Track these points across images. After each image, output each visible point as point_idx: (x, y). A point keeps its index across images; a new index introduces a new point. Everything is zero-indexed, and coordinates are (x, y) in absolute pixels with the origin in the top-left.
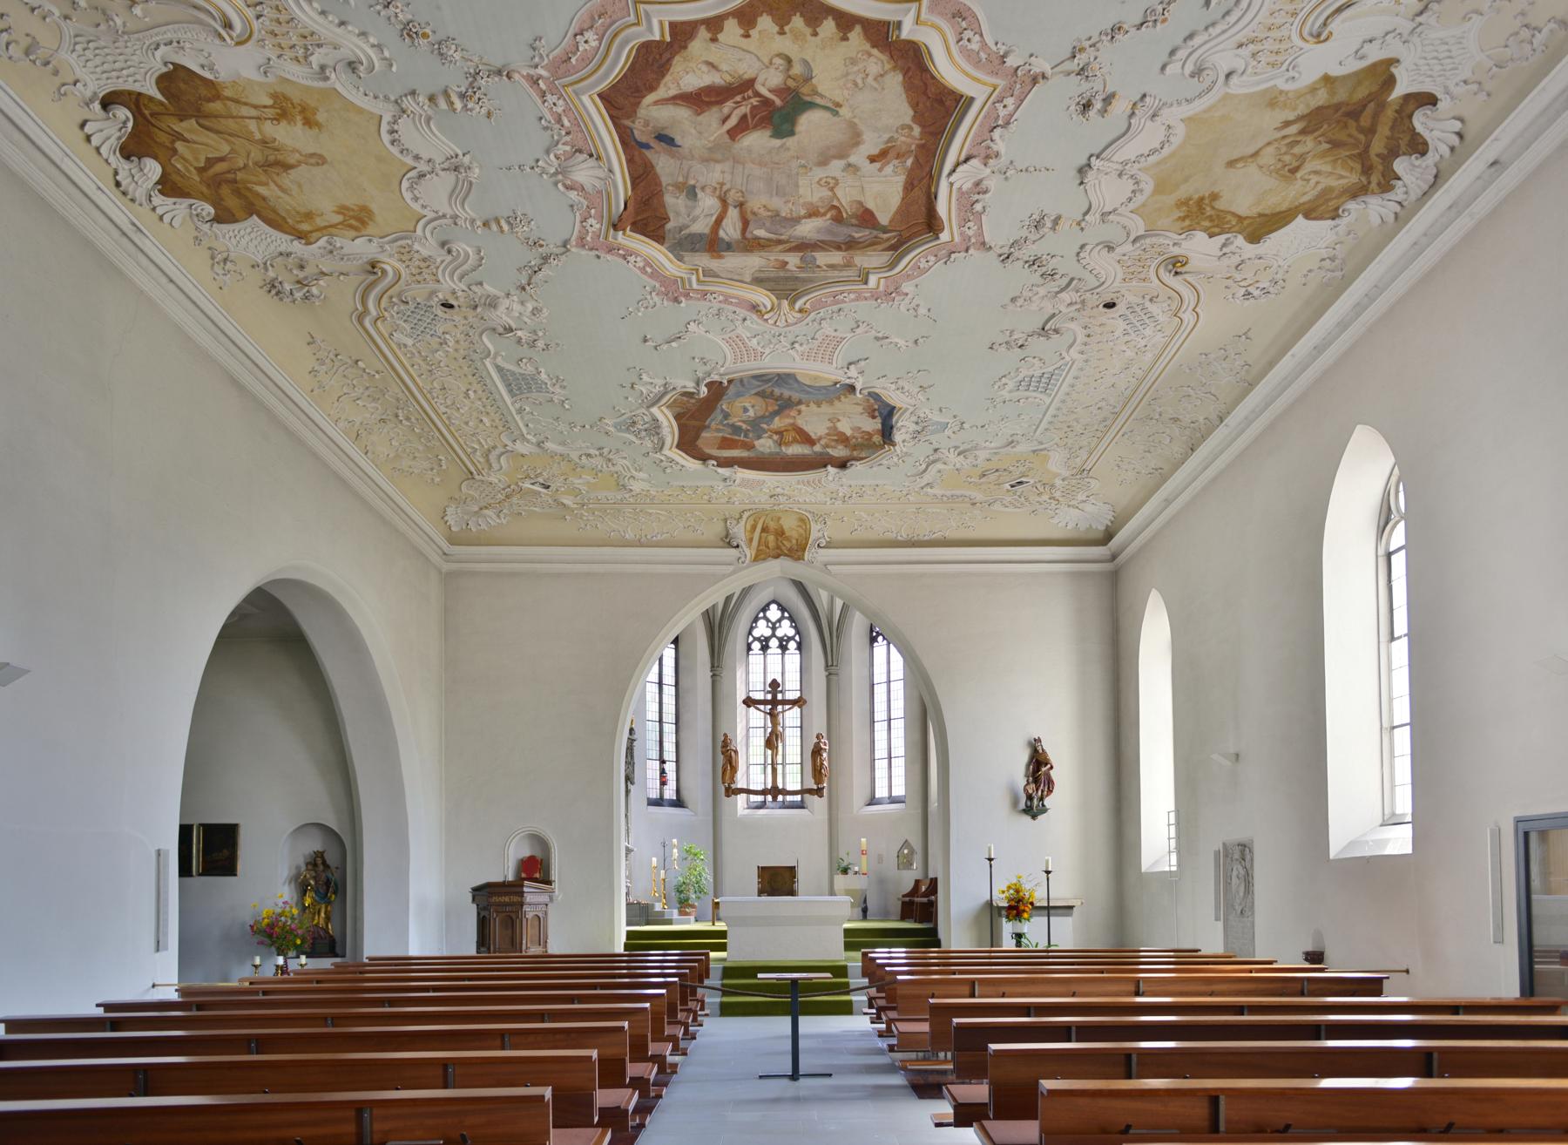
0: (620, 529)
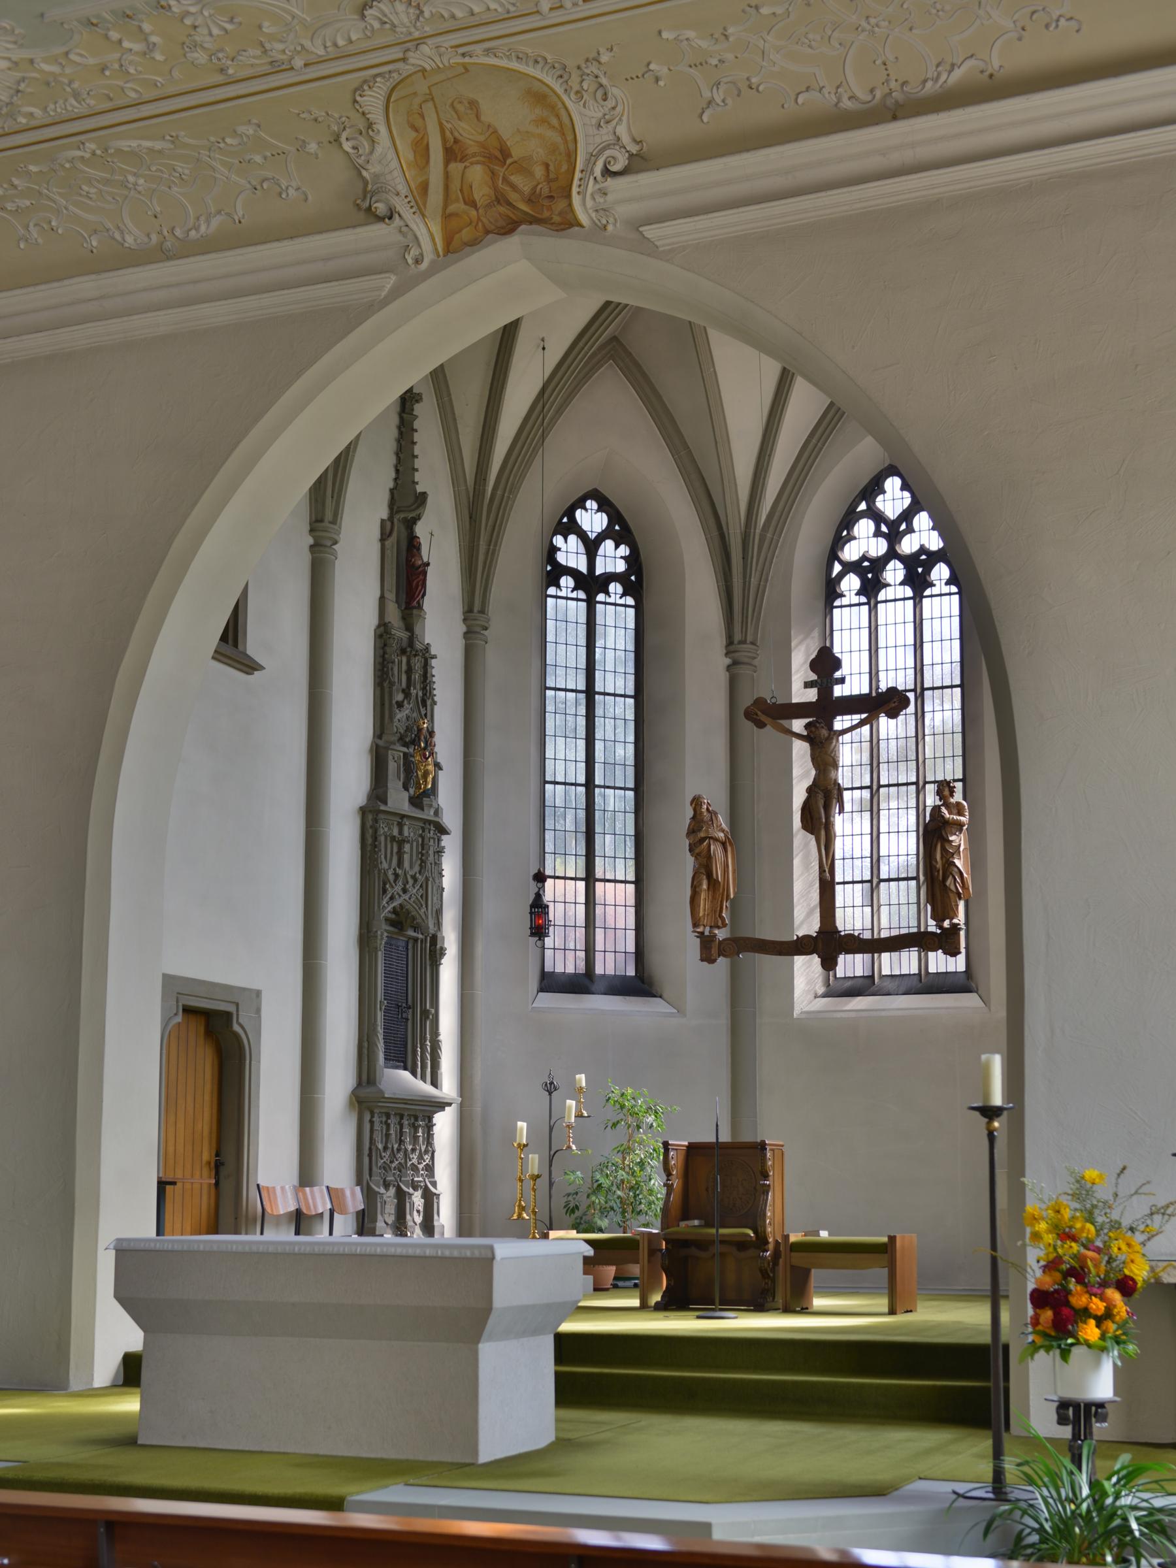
0: (110, 225)
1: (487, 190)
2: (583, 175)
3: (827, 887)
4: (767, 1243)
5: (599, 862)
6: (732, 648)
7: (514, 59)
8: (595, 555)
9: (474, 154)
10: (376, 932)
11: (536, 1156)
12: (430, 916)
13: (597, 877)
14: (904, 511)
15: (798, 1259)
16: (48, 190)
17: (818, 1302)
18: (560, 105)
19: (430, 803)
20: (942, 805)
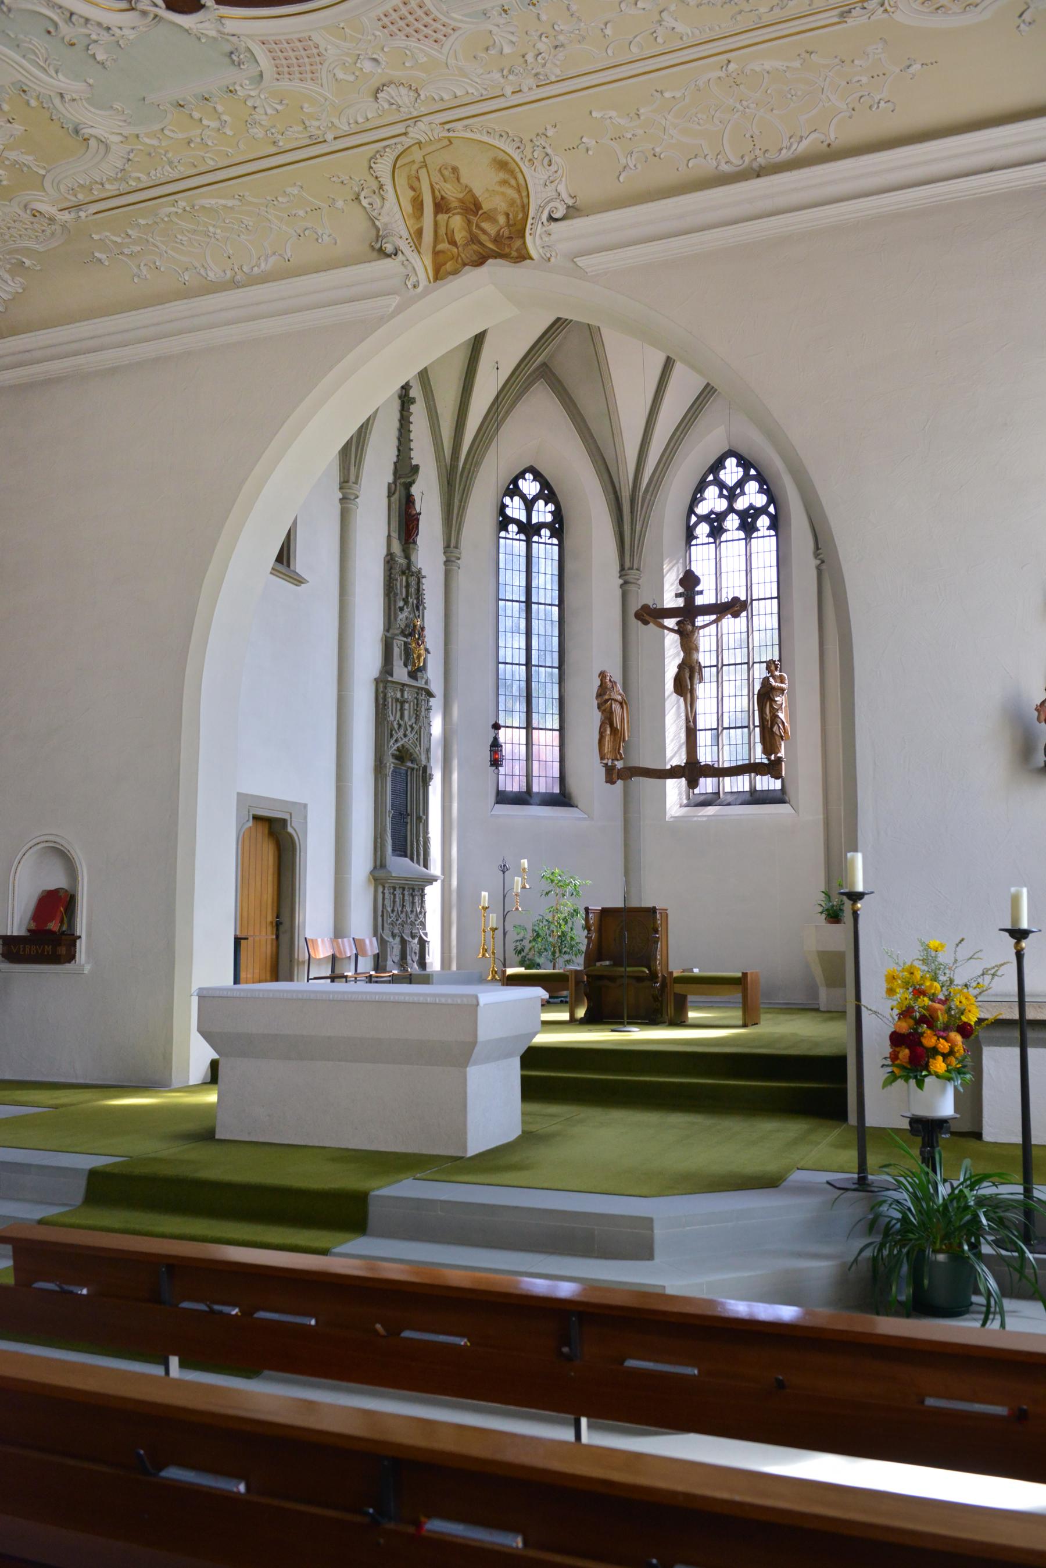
0: (197, 264)
1: (464, 233)
2: (534, 221)
3: (691, 733)
4: (658, 977)
6: (623, 573)
7: (485, 133)
8: (532, 510)
9: (455, 208)
11: (495, 915)
12: (422, 753)
15: (679, 988)
16: (153, 238)
17: (692, 1015)
18: (517, 170)
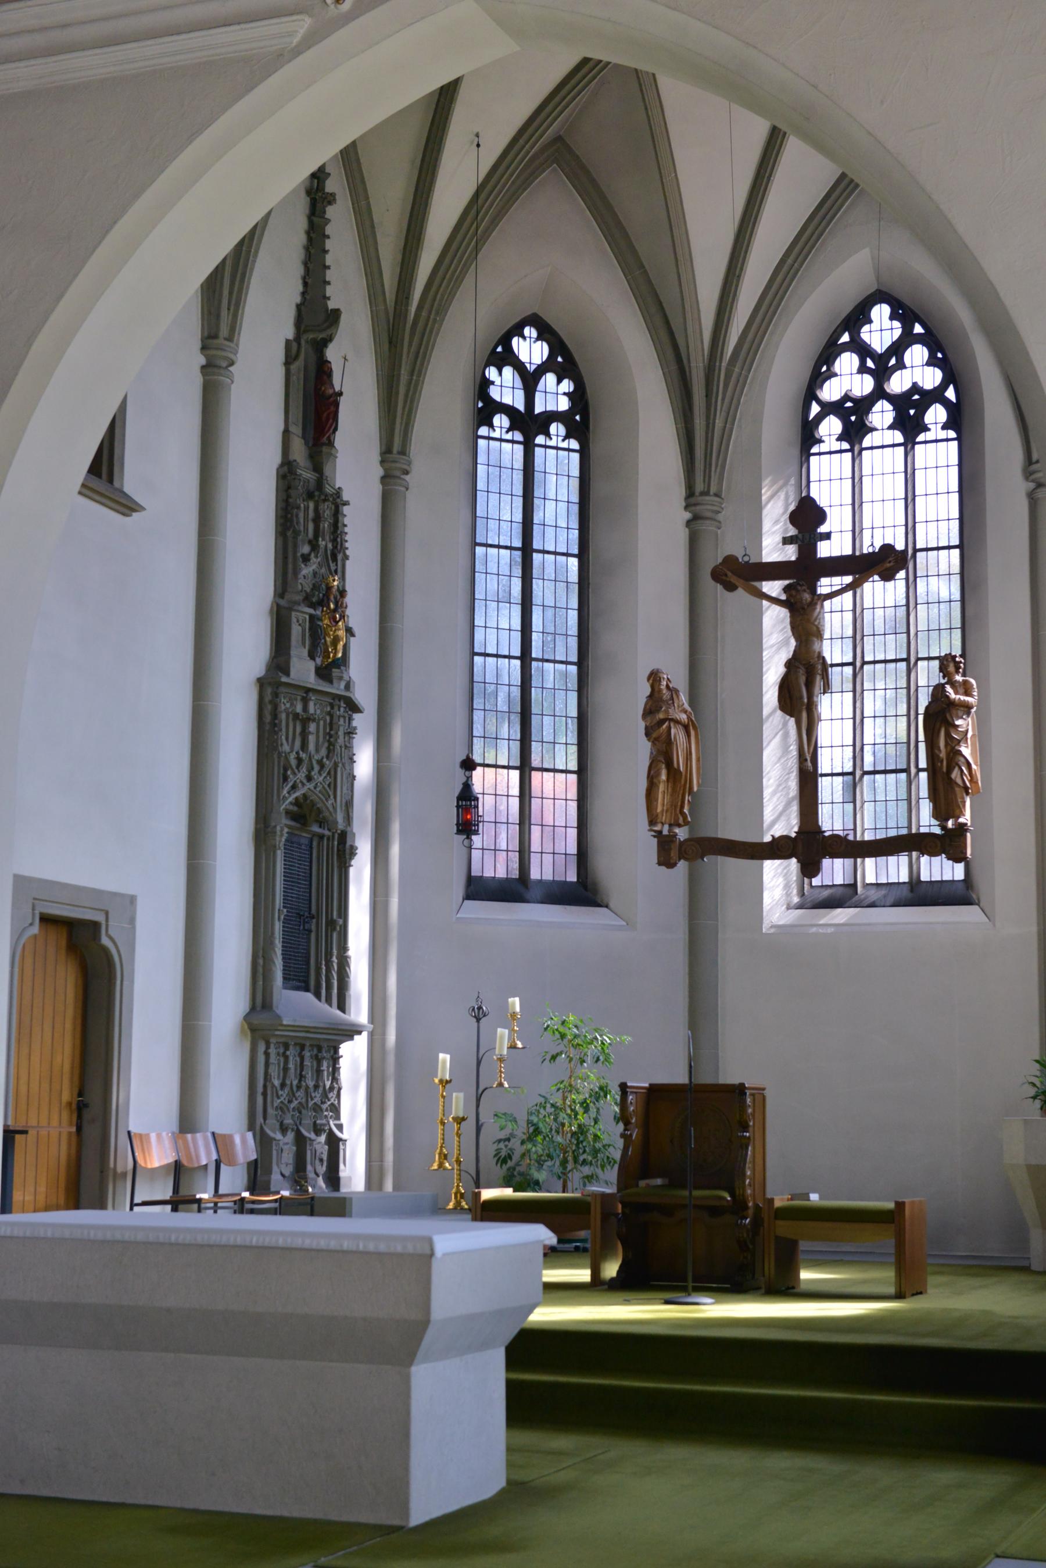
4: (747, 1208)
5: (535, 747)
6: (692, 500)
10: (275, 827)
11: (461, 1095)
13: (533, 765)
14: (893, 343)
15: (784, 1228)
17: (805, 1275)
19: (341, 675)
20: (946, 683)
